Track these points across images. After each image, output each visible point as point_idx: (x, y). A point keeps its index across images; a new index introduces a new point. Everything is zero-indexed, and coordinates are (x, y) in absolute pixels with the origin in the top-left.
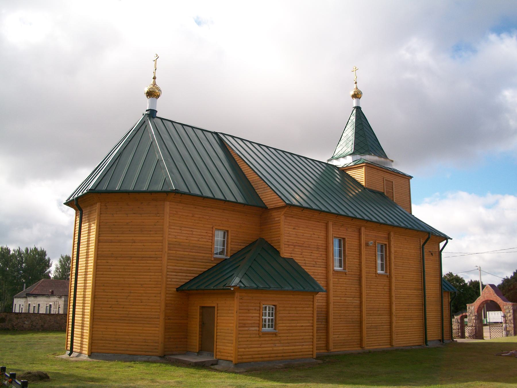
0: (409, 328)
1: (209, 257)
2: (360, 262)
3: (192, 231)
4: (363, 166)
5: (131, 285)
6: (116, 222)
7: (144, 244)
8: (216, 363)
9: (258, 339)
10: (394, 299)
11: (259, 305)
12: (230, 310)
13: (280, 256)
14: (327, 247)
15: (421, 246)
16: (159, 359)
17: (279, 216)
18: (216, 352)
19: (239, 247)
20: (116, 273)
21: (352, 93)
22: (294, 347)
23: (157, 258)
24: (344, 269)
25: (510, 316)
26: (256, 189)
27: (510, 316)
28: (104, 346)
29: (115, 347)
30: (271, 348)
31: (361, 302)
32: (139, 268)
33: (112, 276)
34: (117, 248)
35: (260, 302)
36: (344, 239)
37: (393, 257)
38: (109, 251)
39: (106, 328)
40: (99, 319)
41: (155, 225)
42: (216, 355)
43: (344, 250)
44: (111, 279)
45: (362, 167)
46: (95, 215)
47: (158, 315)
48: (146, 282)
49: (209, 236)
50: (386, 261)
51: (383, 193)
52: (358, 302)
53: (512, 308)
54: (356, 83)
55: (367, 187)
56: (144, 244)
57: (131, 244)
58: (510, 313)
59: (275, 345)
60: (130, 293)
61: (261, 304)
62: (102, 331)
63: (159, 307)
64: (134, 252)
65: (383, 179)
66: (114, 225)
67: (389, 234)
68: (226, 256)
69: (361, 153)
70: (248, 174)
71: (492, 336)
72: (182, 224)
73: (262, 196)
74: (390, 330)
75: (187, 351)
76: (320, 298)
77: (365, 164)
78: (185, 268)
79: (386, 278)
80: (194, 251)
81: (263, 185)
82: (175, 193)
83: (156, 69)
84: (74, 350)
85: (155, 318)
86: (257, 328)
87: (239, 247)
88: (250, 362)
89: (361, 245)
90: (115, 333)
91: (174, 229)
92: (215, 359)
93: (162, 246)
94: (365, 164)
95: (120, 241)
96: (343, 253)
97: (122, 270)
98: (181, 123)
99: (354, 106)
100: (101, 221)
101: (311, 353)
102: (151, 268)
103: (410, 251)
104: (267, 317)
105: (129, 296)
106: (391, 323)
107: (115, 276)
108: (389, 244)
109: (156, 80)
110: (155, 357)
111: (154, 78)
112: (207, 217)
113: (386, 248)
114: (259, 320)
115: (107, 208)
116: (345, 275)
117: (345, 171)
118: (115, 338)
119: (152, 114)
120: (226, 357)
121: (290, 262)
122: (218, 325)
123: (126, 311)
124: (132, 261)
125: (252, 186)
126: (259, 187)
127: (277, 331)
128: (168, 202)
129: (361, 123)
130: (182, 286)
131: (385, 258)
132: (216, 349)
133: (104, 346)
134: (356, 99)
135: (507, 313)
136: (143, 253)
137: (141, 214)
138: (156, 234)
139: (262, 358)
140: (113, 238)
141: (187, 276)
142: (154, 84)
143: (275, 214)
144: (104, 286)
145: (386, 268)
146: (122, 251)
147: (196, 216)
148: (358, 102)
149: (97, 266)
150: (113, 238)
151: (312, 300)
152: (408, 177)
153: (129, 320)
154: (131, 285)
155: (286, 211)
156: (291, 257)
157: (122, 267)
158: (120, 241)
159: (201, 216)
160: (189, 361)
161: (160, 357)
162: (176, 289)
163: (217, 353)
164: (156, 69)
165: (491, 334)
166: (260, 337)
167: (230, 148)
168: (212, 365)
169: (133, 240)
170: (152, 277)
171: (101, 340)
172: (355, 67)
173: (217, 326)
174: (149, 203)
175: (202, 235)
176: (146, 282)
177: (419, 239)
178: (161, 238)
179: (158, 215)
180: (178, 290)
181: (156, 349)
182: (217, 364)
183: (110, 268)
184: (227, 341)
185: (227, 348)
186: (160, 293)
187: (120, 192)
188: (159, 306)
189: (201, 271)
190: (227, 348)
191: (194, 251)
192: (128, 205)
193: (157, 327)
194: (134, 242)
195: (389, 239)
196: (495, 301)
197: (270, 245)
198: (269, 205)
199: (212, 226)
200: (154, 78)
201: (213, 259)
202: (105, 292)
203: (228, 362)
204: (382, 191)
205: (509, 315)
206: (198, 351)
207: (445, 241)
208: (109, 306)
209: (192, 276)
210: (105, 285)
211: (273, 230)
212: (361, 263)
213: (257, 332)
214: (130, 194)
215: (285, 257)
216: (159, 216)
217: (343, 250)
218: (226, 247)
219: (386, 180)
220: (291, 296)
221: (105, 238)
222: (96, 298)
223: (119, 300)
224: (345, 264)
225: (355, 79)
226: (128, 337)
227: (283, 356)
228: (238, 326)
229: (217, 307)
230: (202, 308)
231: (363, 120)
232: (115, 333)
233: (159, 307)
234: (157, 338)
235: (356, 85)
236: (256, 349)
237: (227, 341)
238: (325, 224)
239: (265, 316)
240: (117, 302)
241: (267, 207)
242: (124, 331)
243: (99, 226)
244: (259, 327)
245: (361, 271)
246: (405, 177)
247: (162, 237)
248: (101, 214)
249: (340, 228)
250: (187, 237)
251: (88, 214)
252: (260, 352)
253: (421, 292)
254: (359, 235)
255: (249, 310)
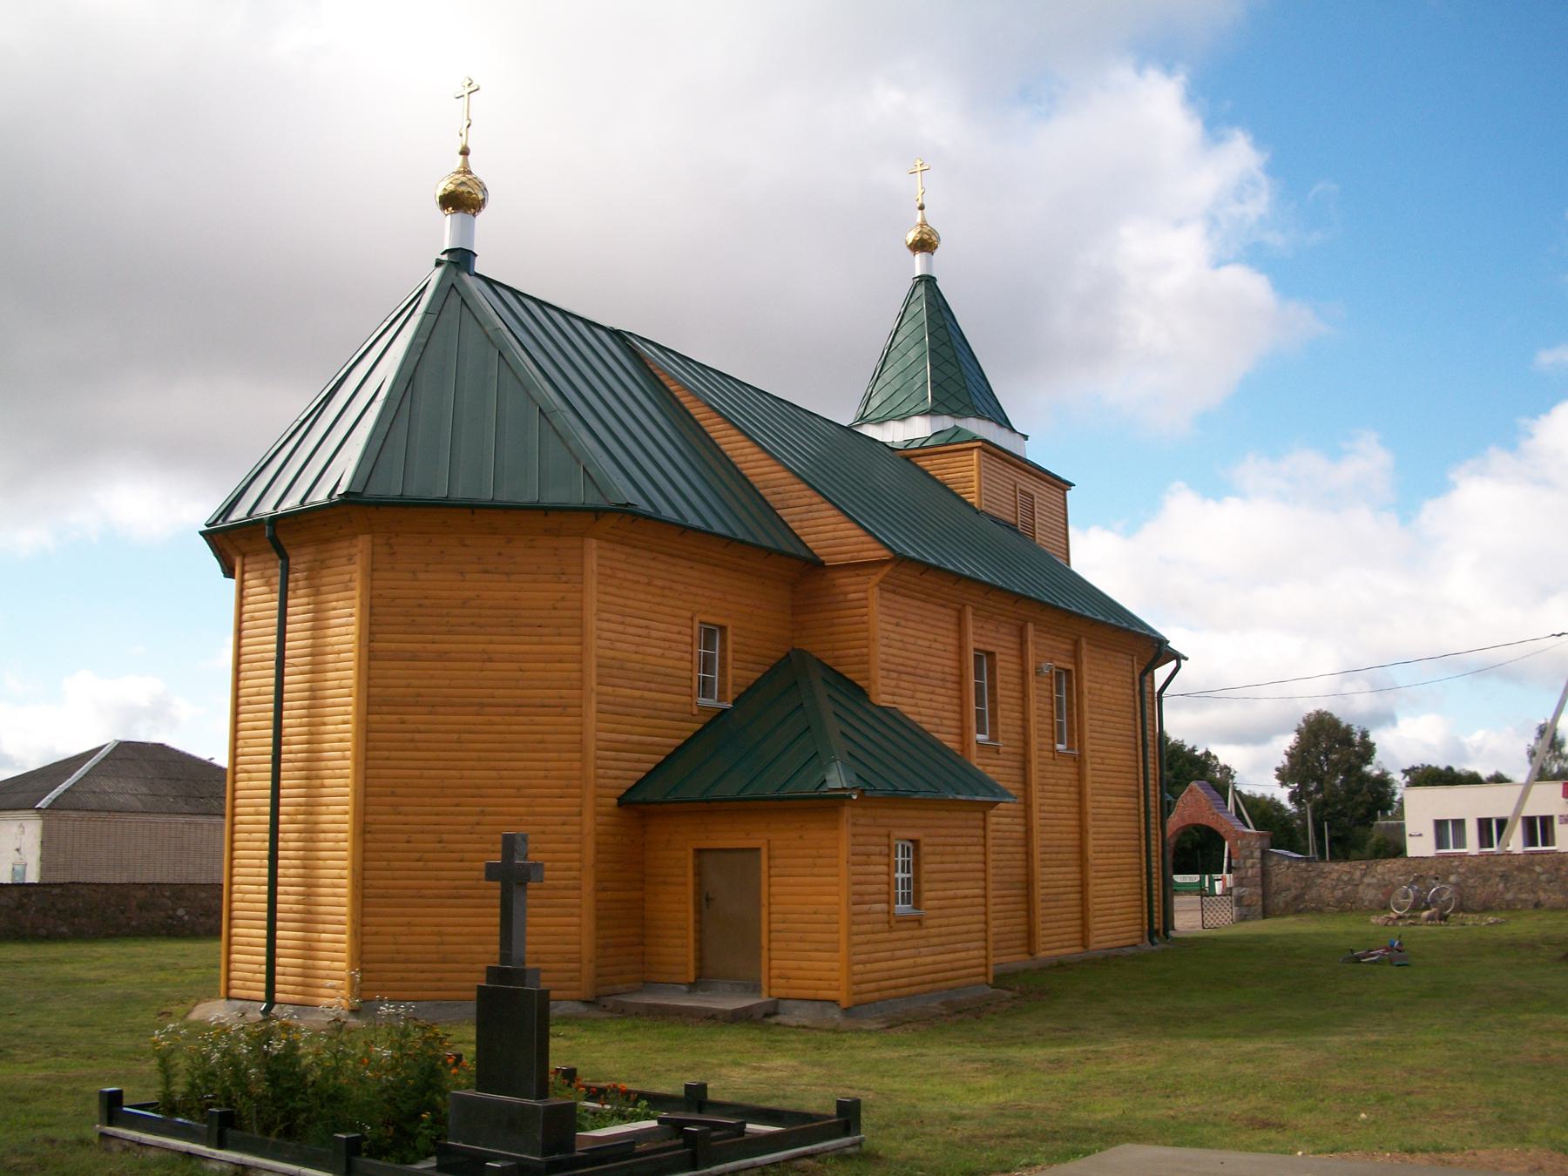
0: (1117, 898)
1: (685, 704)
2: (1025, 720)
3: (647, 627)
4: (972, 448)
5: (484, 791)
6: (426, 598)
7: (524, 666)
8: (772, 1010)
9: (886, 935)
10: (1090, 822)
11: (885, 840)
12: (820, 857)
13: (869, 701)
14: (961, 676)
15: (1137, 676)
16: (582, 1008)
17: (864, 587)
18: (770, 978)
19: (749, 674)
20: (433, 754)
21: (912, 236)
22: (951, 956)
23: (565, 707)
24: (993, 738)
25: (1252, 867)
26: (779, 506)
27: (1252, 867)
28: (402, 980)
29: (440, 980)
30: (912, 960)
31: (1028, 831)
32: (509, 737)
33: (421, 763)
34: (432, 677)
35: (889, 832)
36: (991, 655)
37: (1086, 703)
38: (408, 686)
39: (409, 925)
40: (383, 897)
41: (555, 608)
42: (770, 987)
43: (992, 687)
44: (417, 773)
45: (970, 452)
46: (355, 573)
47: (575, 879)
48: (533, 782)
49: (686, 644)
50: (1070, 715)
51: (1016, 525)
52: (1021, 828)
53: (1259, 843)
54: (922, 208)
55: (983, 508)
56: (524, 666)
57: (477, 665)
58: (1252, 858)
59: (920, 952)
60: (483, 813)
61: (892, 837)
62: (394, 934)
63: (577, 856)
64: (490, 691)
65: (1015, 487)
66: (420, 606)
67: (1076, 643)
68: (719, 701)
69: (953, 413)
70: (745, 462)
71: (1206, 922)
72: (625, 606)
73: (801, 528)
74: (1082, 906)
75: (645, 982)
76: (1003, 821)
77: (979, 444)
78: (635, 738)
79: (1071, 763)
80: (653, 686)
81: (805, 496)
82: (620, 515)
83: (469, 126)
84: (279, 996)
85: (566, 888)
86: (884, 906)
87: (749, 674)
88: (873, 1002)
89: (1028, 673)
90: (437, 939)
91: (608, 621)
92: (764, 998)
93: (581, 671)
94: (979, 444)
95: (442, 657)
96: (989, 694)
97: (406, 745)
98: (534, 296)
99: (918, 274)
100: (376, 592)
101: (982, 970)
102: (548, 737)
103: (1115, 689)
104: (899, 875)
105: (478, 824)
106: (1083, 886)
107: (430, 764)
108: (1078, 670)
109: (469, 157)
110: (570, 1004)
111: (465, 152)
112: (681, 587)
113: (1069, 682)
114: (889, 884)
115: (394, 553)
116: (996, 756)
117: (913, 460)
118: (438, 953)
119: (460, 259)
120: (814, 992)
121: (891, 715)
122: (772, 900)
123: (471, 870)
124: (486, 718)
125: (762, 497)
126: (791, 502)
127: (922, 912)
128: (594, 541)
129: (942, 323)
130: (630, 790)
131: (1067, 709)
132: (770, 969)
133: (402, 980)
134: (924, 253)
135: (1245, 858)
136: (518, 692)
137: (507, 574)
138: (559, 635)
139: (895, 987)
140: (419, 646)
141: (639, 761)
142: (466, 171)
143: (845, 581)
144: (393, 794)
145: (1070, 735)
146: (449, 687)
147: (659, 583)
148: (929, 264)
149: (367, 732)
150: (419, 646)
151: (981, 823)
152: (1063, 485)
153: (483, 897)
154: (484, 791)
155: (886, 576)
156: (893, 706)
157: (455, 736)
158: (442, 657)
159: (667, 584)
160: (707, 1010)
161: (586, 1002)
162: (618, 799)
163: (773, 981)
164: (469, 126)
165: (1206, 915)
166: (891, 929)
167: (672, 382)
168: (767, 1015)
169: (484, 652)
170: (550, 765)
171: (392, 961)
172: (919, 162)
173: (770, 904)
174: (532, 540)
175: (669, 641)
176: (533, 782)
177: (1130, 658)
178: (576, 648)
179: (564, 578)
180: (622, 802)
181: (571, 979)
182: (775, 1013)
183: (412, 740)
184: (814, 946)
185: (816, 965)
186: (580, 814)
187: (453, 506)
188: (579, 851)
189: (670, 746)
190: (816, 965)
191: (653, 686)
192: (464, 545)
193: (572, 915)
194: (491, 660)
195: (1075, 656)
196: (1212, 826)
197: (832, 669)
198: (829, 554)
199: (689, 614)
200: (465, 152)
201: (695, 711)
202: (399, 814)
203: (818, 1003)
204: (1013, 520)
205: (1249, 862)
206: (692, 979)
207: (1173, 664)
208: (416, 855)
209: (650, 761)
210: (399, 791)
211: (842, 629)
212: (1028, 720)
213: (885, 917)
214: (476, 511)
215: (883, 704)
216: (566, 582)
217: (989, 688)
218: (720, 675)
219: (1022, 492)
220: (946, 814)
221: (393, 646)
222: (369, 832)
223: (445, 837)
224: (994, 724)
225: (919, 196)
226: (480, 948)
227: (934, 982)
228: (850, 903)
229: (769, 850)
230: (699, 852)
231: (946, 315)
232: (437, 939)
233: (577, 856)
234: (575, 948)
235: (923, 214)
236: (883, 965)
237: (814, 946)
238: (953, 613)
239: (1544, 844)
240: (440, 842)
241: (823, 562)
242: (467, 930)
243: (371, 607)
244: (888, 903)
245: (1026, 743)
246: (1058, 483)
247: (580, 644)
248: (373, 570)
249: (986, 626)
250: (638, 645)
251: (310, 570)
252: (893, 974)
253: (1135, 800)
254: (1021, 644)
255: (868, 855)
